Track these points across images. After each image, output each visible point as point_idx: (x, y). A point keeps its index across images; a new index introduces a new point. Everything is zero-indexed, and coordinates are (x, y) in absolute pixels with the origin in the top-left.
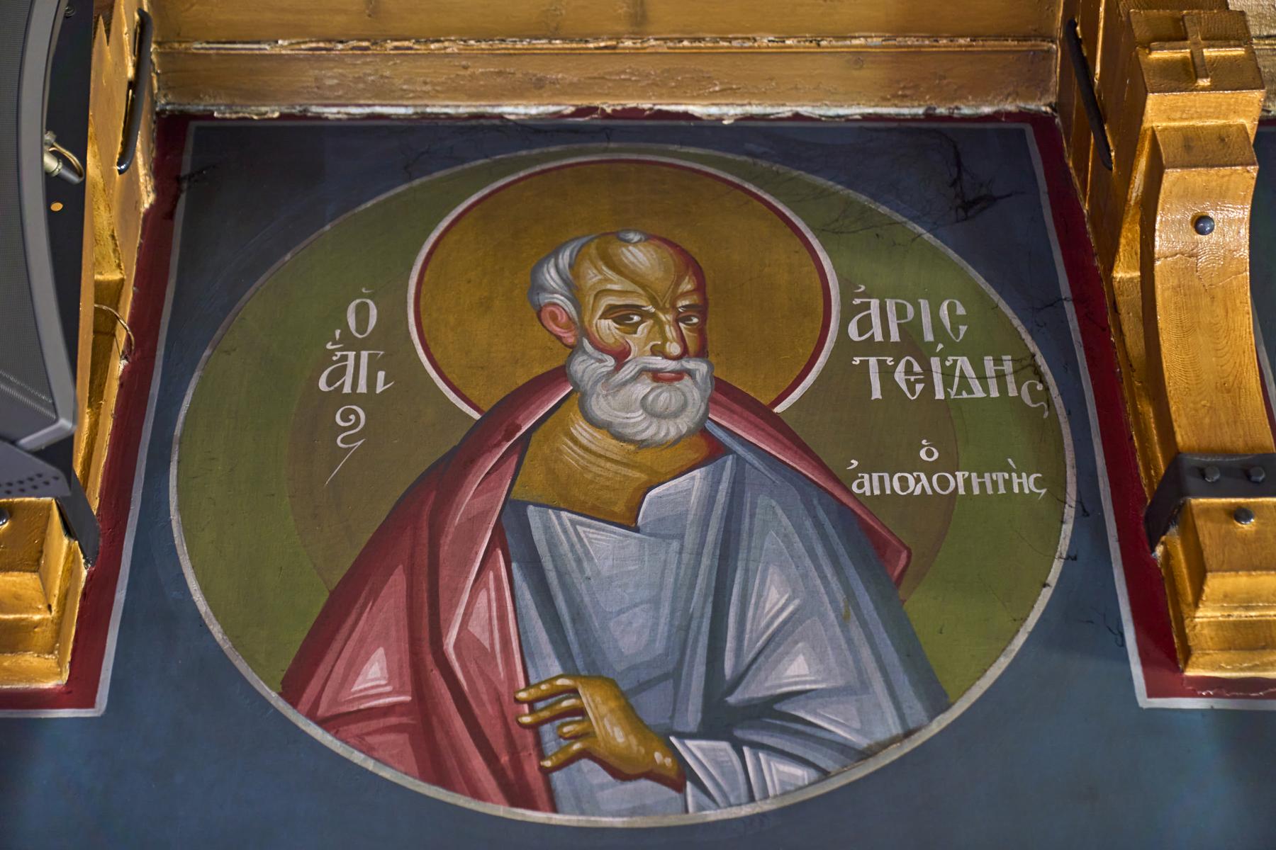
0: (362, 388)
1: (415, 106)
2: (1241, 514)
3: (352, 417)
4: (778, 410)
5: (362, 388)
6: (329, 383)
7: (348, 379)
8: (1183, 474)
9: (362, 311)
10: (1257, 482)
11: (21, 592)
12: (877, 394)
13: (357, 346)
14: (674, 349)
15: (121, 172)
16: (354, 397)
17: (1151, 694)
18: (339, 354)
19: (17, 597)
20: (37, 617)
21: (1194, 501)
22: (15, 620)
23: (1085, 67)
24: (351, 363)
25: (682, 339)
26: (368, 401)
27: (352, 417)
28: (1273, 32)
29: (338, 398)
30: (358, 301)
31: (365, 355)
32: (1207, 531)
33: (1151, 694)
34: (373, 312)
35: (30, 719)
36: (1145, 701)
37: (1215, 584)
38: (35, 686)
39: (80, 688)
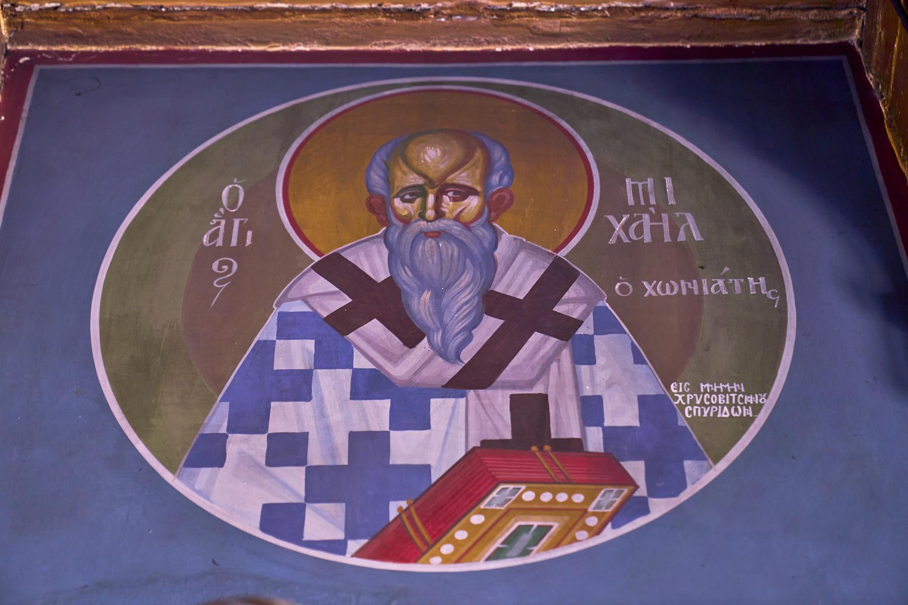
0: (234, 242)
3: (225, 267)
26: (239, 252)
31: (237, 222)
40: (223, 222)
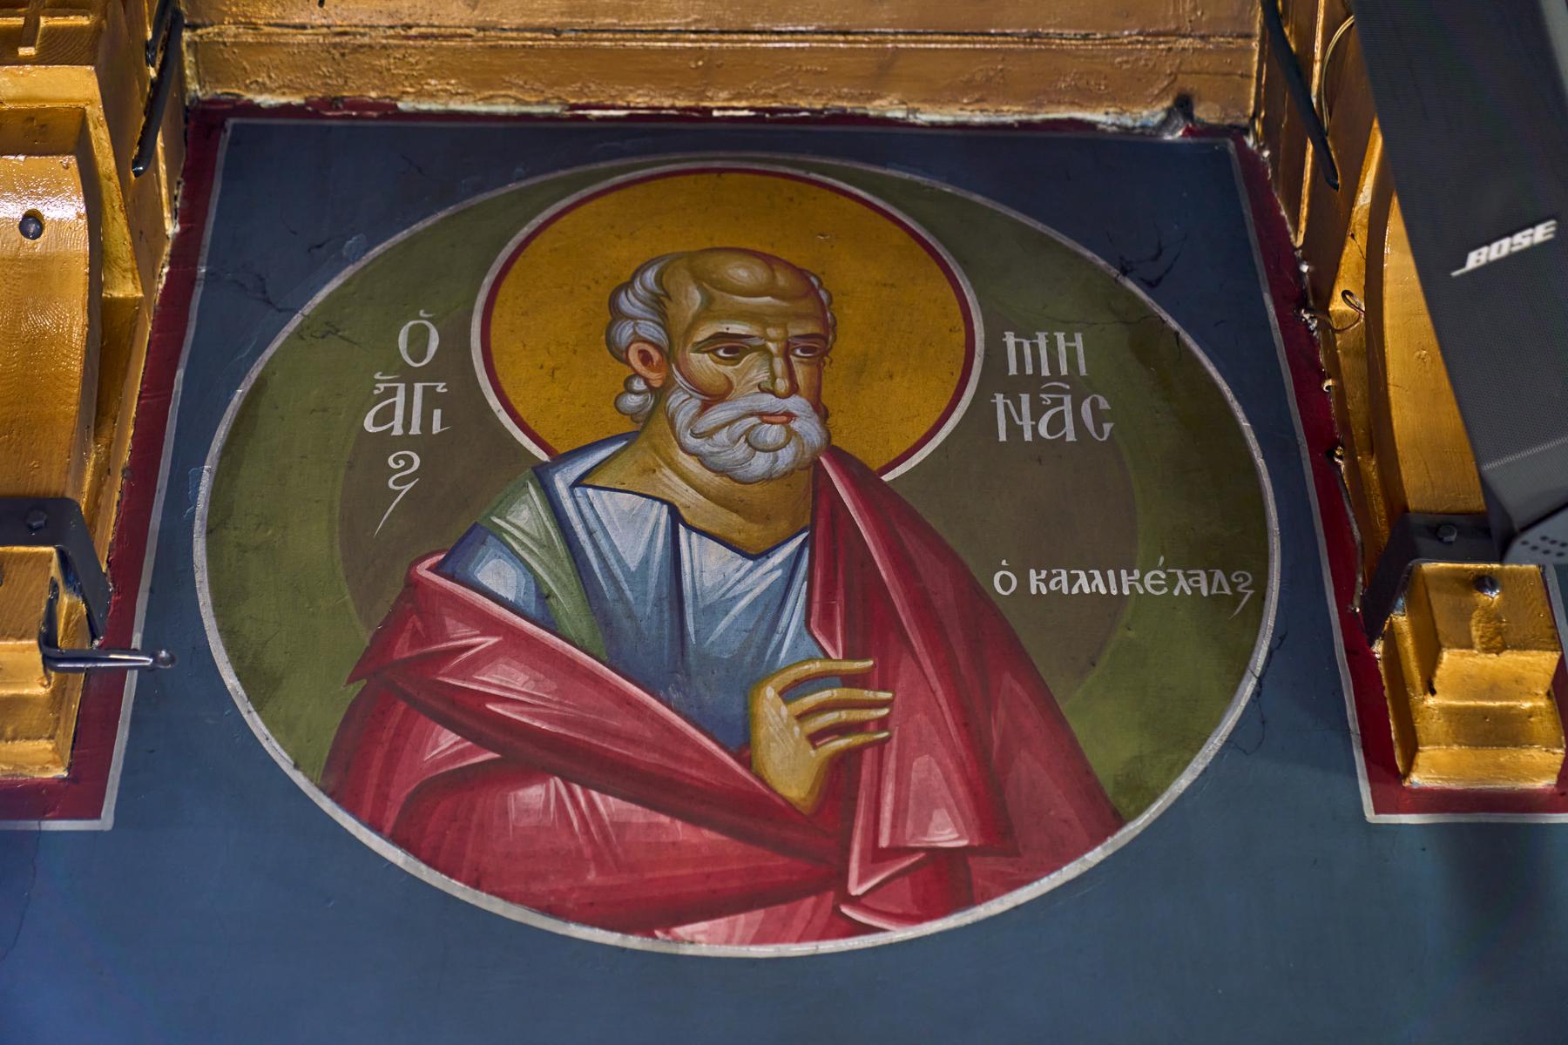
0: (415, 430)
1: (518, 101)
2: (1483, 582)
4: (886, 478)
5: (415, 430)
6: (395, 483)
7: (399, 412)
8: (1417, 533)
9: (418, 351)
10: (31, 529)
11: (1527, 674)
12: (1003, 437)
13: (409, 377)
14: (782, 385)
15: (137, 174)
16: (406, 441)
17: (1378, 811)
18: (382, 386)
19: (1518, 680)
20: (1527, 705)
21: (1429, 567)
22: (1501, 708)
23: (1299, 67)
24: (400, 399)
25: (791, 374)
27: (402, 463)
28: (148, 5)
29: (386, 443)
30: (425, 362)
31: (418, 387)
32: (1441, 603)
33: (1378, 811)
34: (434, 344)
35: (1529, 825)
36: (1371, 816)
37: (1450, 659)
38: (1528, 785)
39: (79, 793)
40: (401, 387)
